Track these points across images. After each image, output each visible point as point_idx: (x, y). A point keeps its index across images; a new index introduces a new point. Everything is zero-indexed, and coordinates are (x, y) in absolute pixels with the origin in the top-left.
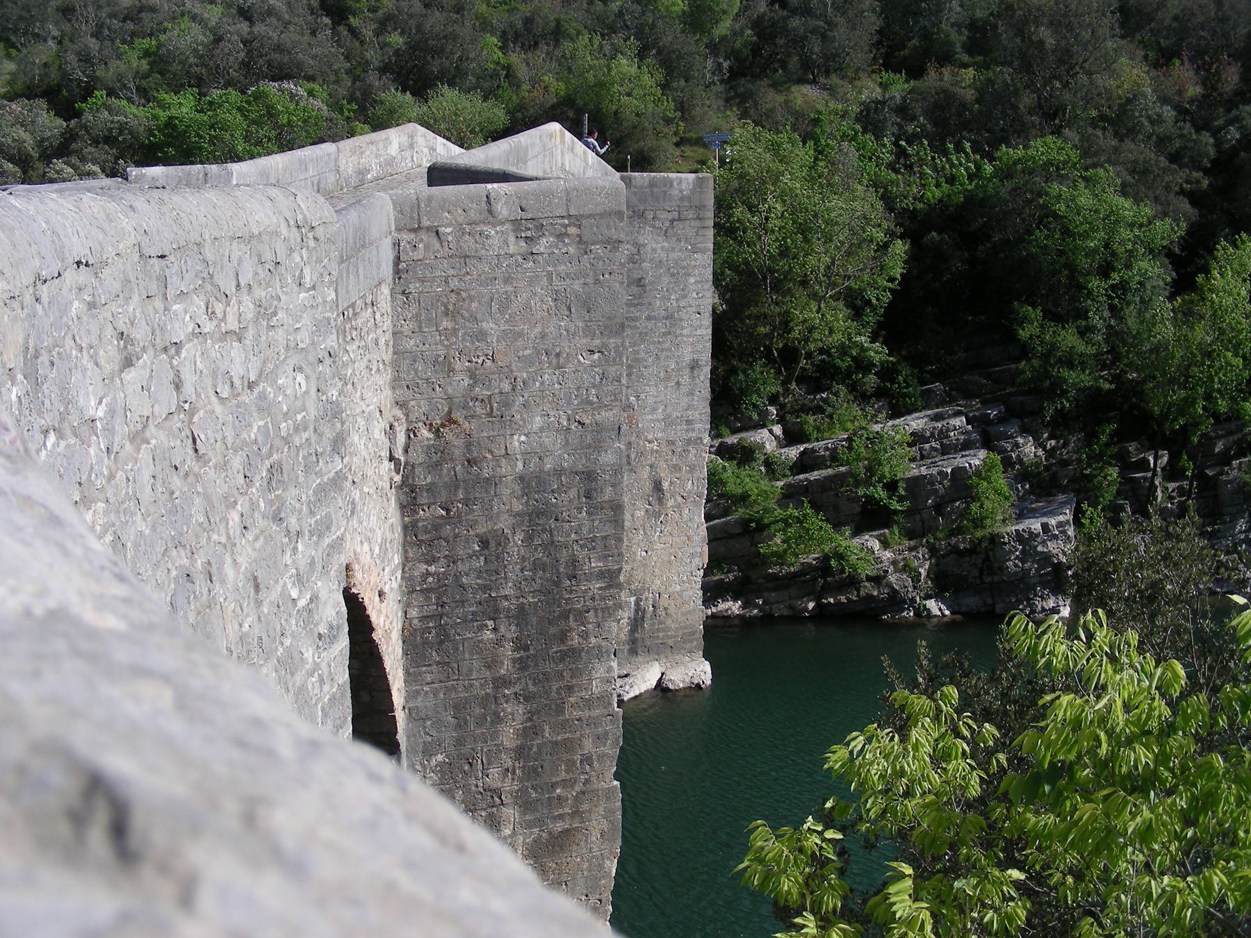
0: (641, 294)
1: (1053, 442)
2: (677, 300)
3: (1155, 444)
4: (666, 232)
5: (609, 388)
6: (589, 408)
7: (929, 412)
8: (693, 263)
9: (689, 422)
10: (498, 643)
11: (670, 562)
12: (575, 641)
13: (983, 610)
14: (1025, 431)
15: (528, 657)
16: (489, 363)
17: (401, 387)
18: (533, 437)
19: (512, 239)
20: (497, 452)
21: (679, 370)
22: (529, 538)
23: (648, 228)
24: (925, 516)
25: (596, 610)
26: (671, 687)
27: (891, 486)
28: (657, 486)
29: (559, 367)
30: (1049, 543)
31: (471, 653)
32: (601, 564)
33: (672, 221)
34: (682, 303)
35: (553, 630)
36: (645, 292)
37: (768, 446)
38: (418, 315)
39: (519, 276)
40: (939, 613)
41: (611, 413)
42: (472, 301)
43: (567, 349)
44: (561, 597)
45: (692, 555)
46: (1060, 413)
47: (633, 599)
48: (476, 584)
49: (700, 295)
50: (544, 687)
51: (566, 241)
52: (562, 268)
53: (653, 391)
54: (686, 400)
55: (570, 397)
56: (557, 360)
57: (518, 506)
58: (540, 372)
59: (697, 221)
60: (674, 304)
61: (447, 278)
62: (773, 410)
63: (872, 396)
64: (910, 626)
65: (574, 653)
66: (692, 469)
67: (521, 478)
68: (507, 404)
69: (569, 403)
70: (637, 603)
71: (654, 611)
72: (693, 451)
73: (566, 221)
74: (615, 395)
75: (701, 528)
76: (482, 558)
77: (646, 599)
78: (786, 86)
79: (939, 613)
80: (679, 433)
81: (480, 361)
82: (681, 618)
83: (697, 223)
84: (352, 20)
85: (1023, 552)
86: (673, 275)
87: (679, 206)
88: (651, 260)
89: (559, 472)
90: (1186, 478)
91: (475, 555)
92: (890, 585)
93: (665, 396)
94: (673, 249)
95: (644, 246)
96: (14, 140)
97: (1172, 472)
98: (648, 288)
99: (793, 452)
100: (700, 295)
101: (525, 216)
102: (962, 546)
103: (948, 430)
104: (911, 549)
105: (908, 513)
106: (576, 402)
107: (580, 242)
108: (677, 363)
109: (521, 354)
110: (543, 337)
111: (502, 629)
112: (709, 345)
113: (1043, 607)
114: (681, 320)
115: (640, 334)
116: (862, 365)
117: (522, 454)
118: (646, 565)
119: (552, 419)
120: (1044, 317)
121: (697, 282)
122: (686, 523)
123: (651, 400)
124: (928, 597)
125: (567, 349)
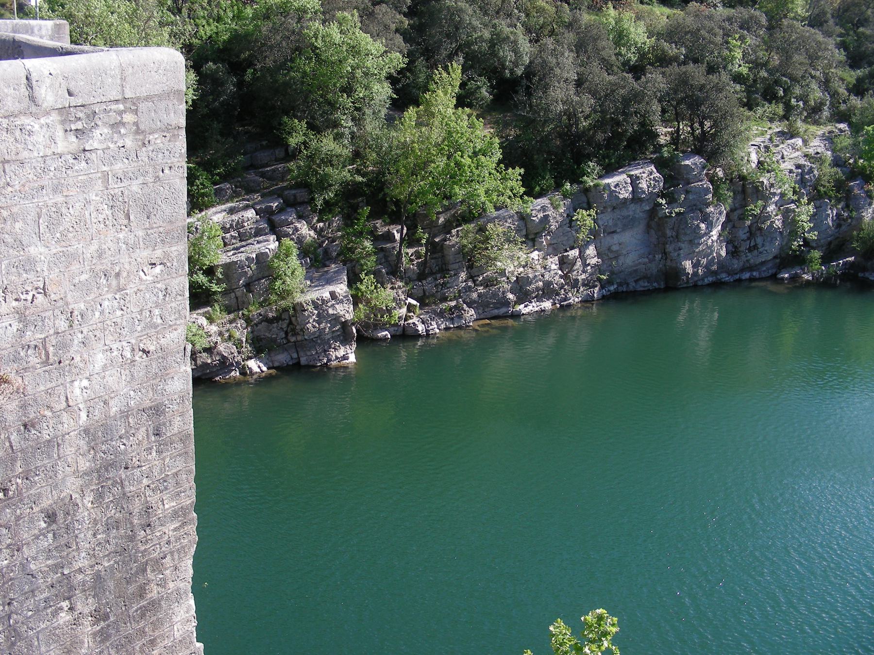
1: (321, 224)
3: (395, 218)
7: (223, 207)
10: (76, 622)
12: (154, 592)
13: (291, 363)
14: (300, 217)
15: (109, 626)
16: (40, 297)
18: (96, 379)
19: (60, 133)
22: (99, 496)
24: (239, 294)
25: (172, 553)
29: (120, 289)
30: (337, 306)
31: (48, 644)
32: (174, 504)
35: (132, 588)
40: (258, 370)
42: (15, 221)
43: (127, 266)
44: (137, 551)
46: (326, 202)
48: (48, 566)
50: (127, 651)
57: (84, 464)
58: (99, 300)
64: (238, 384)
65: (155, 605)
67: (86, 431)
68: (64, 346)
76: (50, 535)
79: (258, 370)
81: (30, 298)
85: (319, 315)
89: (125, 414)
90: (421, 245)
91: (43, 534)
92: (219, 354)
97: (411, 240)
101: (73, 101)
102: (270, 315)
103: (243, 221)
104: (231, 322)
105: (225, 293)
106: (139, 328)
107: (138, 131)
110: (100, 256)
111: (79, 606)
113: (336, 356)
120: (308, 128)
124: (250, 358)
125: (127, 266)
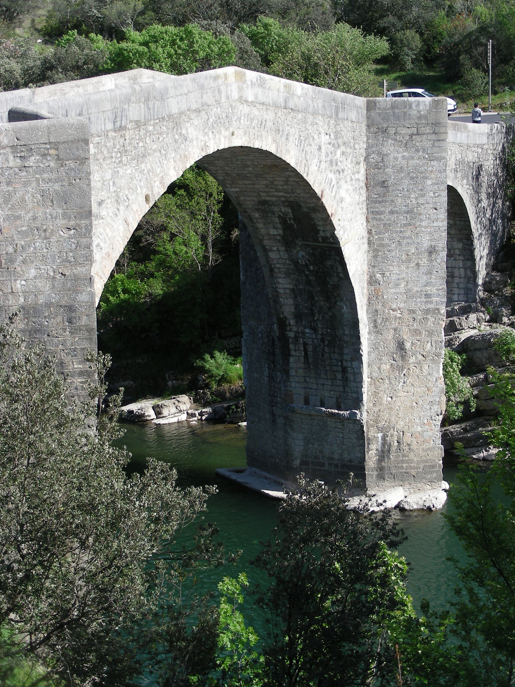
0: (385, 193)
2: (416, 198)
4: (406, 144)
5: (82, 252)
6: (68, 264)
8: (430, 169)
9: (427, 296)
18: (30, 282)
19: (11, 157)
20: (5, 291)
21: (418, 254)
23: (390, 141)
26: (407, 507)
28: (401, 346)
29: (46, 238)
32: (81, 366)
33: (411, 135)
34: (421, 201)
36: (388, 192)
39: (17, 181)
41: (84, 269)
47: (380, 435)
49: (437, 194)
51: (49, 158)
52: (45, 176)
53: (396, 270)
54: (425, 278)
55: (55, 258)
59: (433, 135)
60: (414, 201)
66: (430, 333)
68: (12, 261)
69: (54, 262)
70: (384, 438)
71: (399, 446)
72: (432, 319)
73: (48, 146)
74: (86, 257)
75: (439, 381)
77: (392, 436)
80: (419, 304)
82: (422, 453)
83: (434, 137)
86: (412, 178)
87: (417, 124)
89: (48, 305)
93: (407, 273)
94: (412, 158)
95: (387, 155)
96: (6, 71)
98: (391, 189)
100: (437, 194)
101: (19, 143)
106: (59, 261)
107: (58, 159)
108: (417, 248)
109: (19, 229)
110: (34, 219)
112: (445, 234)
114: (420, 214)
115: (385, 225)
117: (23, 292)
119: (43, 271)
121: (433, 184)
123: (394, 277)
125: (51, 227)
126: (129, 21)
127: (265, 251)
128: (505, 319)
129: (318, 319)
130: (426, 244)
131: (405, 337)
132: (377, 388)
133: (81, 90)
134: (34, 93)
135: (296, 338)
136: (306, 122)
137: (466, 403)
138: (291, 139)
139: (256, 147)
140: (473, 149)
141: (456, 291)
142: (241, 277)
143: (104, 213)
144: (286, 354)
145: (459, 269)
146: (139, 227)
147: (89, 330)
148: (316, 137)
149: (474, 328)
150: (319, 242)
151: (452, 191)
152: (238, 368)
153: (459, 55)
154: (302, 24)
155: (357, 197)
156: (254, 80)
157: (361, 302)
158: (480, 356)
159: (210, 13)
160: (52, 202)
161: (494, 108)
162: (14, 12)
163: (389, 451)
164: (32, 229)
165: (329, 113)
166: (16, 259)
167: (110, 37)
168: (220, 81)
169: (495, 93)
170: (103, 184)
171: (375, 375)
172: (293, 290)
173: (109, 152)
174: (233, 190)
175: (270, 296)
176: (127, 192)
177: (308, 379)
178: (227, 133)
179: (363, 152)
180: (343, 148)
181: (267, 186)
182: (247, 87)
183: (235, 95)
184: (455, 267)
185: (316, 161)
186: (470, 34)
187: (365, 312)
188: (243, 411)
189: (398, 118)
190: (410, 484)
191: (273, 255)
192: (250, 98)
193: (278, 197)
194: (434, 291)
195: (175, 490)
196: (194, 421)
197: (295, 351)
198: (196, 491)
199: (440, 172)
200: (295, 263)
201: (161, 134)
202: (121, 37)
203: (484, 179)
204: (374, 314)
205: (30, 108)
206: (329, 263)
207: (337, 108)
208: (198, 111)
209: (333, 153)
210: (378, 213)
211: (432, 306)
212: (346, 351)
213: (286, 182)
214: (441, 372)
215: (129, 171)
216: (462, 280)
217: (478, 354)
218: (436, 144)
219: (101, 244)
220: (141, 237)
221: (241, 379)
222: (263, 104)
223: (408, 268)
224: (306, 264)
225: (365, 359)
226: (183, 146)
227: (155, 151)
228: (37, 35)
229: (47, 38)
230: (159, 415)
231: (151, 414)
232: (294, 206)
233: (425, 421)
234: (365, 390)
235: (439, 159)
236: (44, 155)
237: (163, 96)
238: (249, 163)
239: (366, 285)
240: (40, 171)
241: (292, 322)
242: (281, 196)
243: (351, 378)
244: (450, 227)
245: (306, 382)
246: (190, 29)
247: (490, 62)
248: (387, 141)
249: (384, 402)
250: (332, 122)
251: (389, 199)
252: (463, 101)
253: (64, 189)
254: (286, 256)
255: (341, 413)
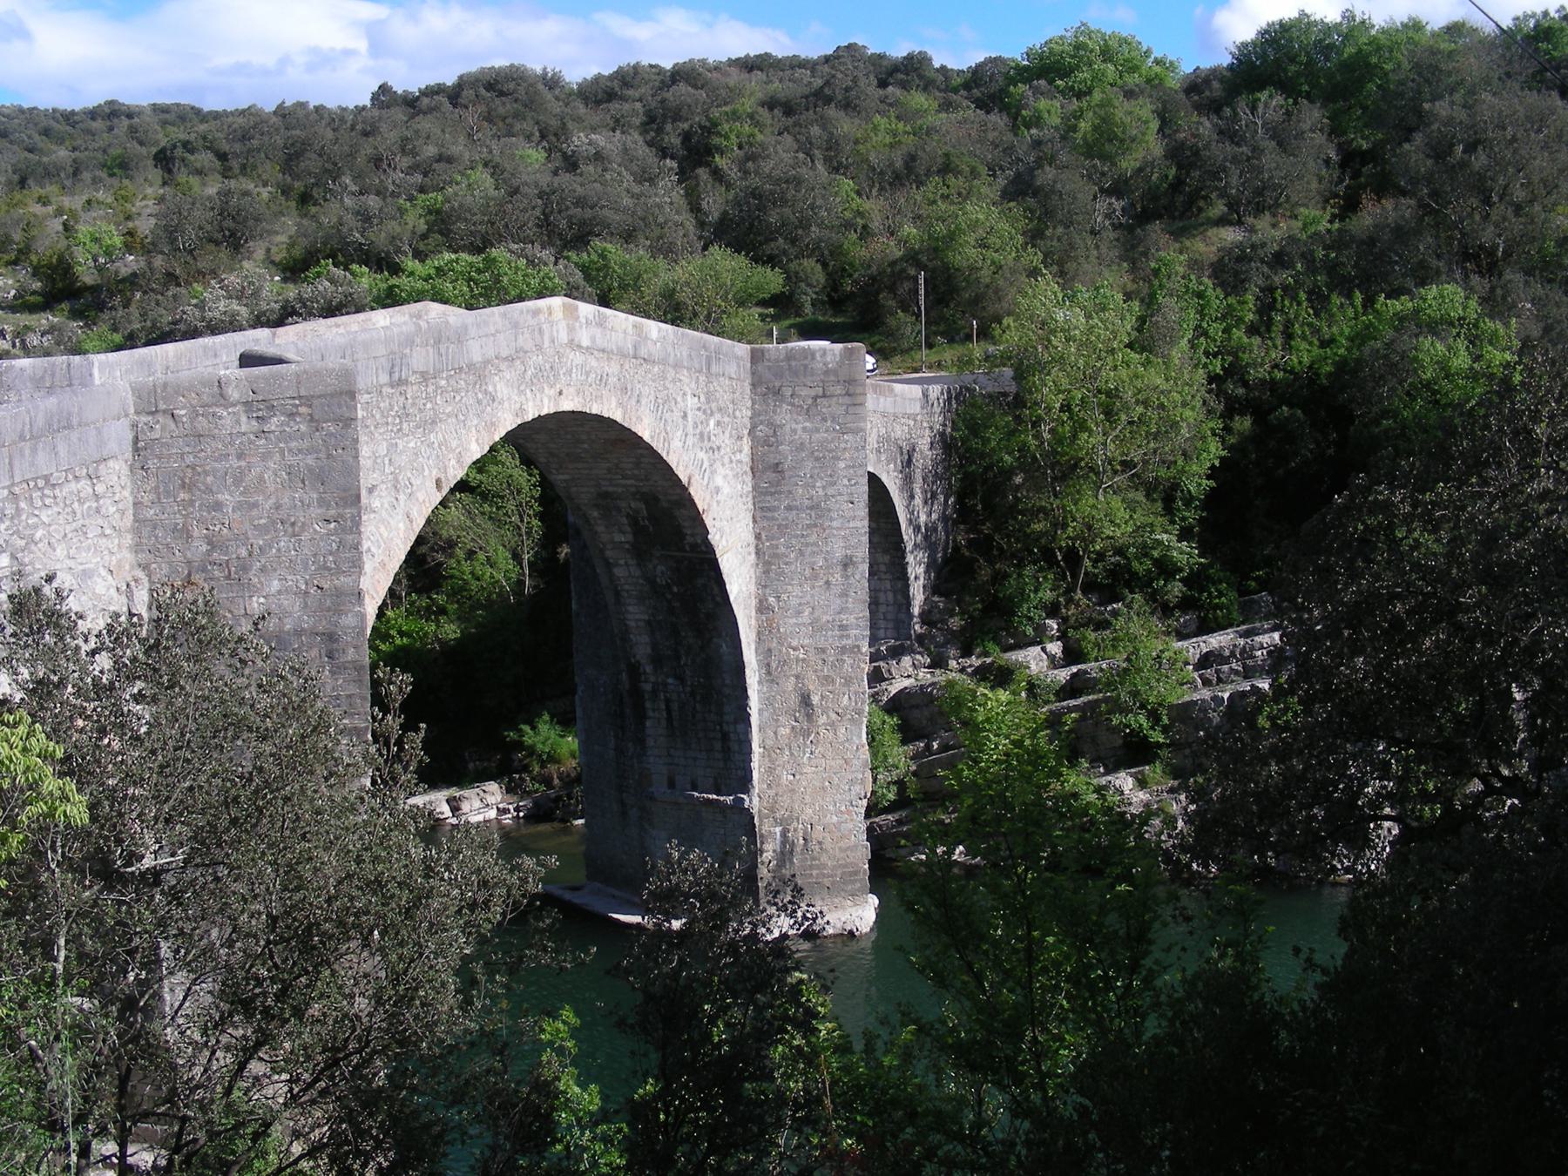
0: (779, 481)
2: (824, 488)
4: (808, 410)
6: (326, 573)
8: (843, 445)
9: (842, 627)
11: (824, 788)
17: (142, 551)
19: (244, 419)
21: (827, 568)
27: (1154, 716)
28: (806, 701)
33: (815, 398)
34: (831, 491)
37: (1033, 666)
38: (157, 487)
45: (852, 782)
47: (778, 830)
53: (797, 591)
54: (838, 602)
56: (295, 530)
60: (821, 492)
61: (182, 455)
62: (1053, 624)
63: (1176, 607)
66: (848, 682)
68: (245, 568)
69: (306, 568)
70: (784, 834)
71: (805, 845)
72: (849, 661)
75: (862, 750)
77: (795, 830)
78: (1202, 229)
83: (847, 400)
84: (717, 158)
86: (817, 459)
88: (791, 442)
89: (298, 633)
93: (812, 596)
94: (817, 430)
95: (782, 426)
98: (787, 474)
99: (1063, 675)
103: (1253, 648)
104: (1172, 791)
107: (312, 419)
109: (256, 523)
110: (277, 508)
112: (865, 539)
114: (830, 510)
116: (1166, 568)
118: (793, 790)
121: (848, 467)
122: (842, 743)
123: (794, 602)
125: (302, 519)
126: (406, 248)
127: (608, 565)
128: (953, 664)
129: (686, 664)
130: (839, 554)
131: (811, 687)
132: (772, 761)
133: (341, 330)
134: (274, 334)
135: (654, 692)
136: (665, 378)
137: (900, 783)
138: (644, 401)
139: (594, 412)
140: (903, 421)
141: (882, 624)
142: (574, 606)
143: (376, 504)
144: (641, 716)
145: (885, 592)
146: (420, 540)
147: (359, 668)
148: (679, 399)
149: (909, 676)
150: (685, 551)
151: (874, 480)
152: (571, 742)
153: (878, 293)
154: (655, 251)
155: (739, 487)
156: (591, 317)
157: (747, 637)
158: (920, 717)
159: (522, 235)
160: (303, 482)
161: (930, 367)
162: (240, 239)
163: (791, 852)
164: (274, 523)
165: (697, 366)
166: (251, 566)
167: (380, 270)
168: (542, 317)
169: (930, 346)
170: (375, 462)
171: (769, 743)
172: (649, 623)
173: (383, 416)
174: (561, 477)
175: (616, 631)
176: (409, 475)
177: (672, 751)
178: (552, 392)
179: (747, 421)
180: (718, 416)
181: (609, 470)
182: (581, 327)
183: (563, 337)
184: (880, 590)
185: (679, 433)
186: (893, 263)
187: (753, 651)
188: (578, 803)
189: (796, 374)
190: (823, 899)
191: (618, 572)
192: (585, 342)
193: (624, 486)
194: (852, 619)
195: (496, 864)
196: (507, 820)
197: (654, 710)
198: (528, 862)
199: (857, 449)
200: (651, 582)
201: (457, 391)
202: (396, 270)
203: (919, 462)
204: (765, 654)
205: (271, 351)
206: (700, 582)
207: (709, 359)
208: (510, 359)
209: (706, 423)
210: (769, 509)
211: (850, 642)
212: (727, 709)
213: (638, 465)
214: (864, 736)
215: (412, 445)
216: (890, 608)
217: (916, 713)
218: (851, 410)
219: (373, 549)
220: (424, 555)
221: (574, 757)
222: (603, 351)
223: (813, 587)
224: (668, 584)
225: (755, 720)
226: (489, 408)
227: (449, 416)
228: (273, 269)
229: (288, 274)
230: (455, 809)
231: (445, 810)
232: (650, 499)
233: (843, 808)
234: (755, 764)
235: (855, 432)
236: (291, 415)
237: (460, 337)
238: (584, 437)
239: (753, 613)
240: (285, 437)
241: (649, 669)
242: (631, 486)
243: (735, 747)
244: (872, 532)
245: (669, 755)
246: (493, 255)
247: (922, 303)
248: (780, 407)
249: (784, 781)
250: (702, 378)
251: (786, 488)
252: (886, 358)
253: (320, 463)
254: (638, 573)
255: (722, 798)
